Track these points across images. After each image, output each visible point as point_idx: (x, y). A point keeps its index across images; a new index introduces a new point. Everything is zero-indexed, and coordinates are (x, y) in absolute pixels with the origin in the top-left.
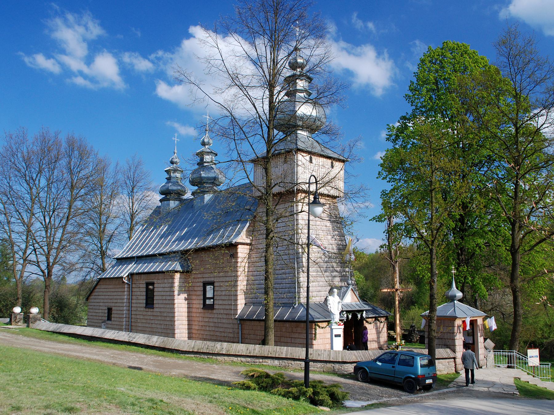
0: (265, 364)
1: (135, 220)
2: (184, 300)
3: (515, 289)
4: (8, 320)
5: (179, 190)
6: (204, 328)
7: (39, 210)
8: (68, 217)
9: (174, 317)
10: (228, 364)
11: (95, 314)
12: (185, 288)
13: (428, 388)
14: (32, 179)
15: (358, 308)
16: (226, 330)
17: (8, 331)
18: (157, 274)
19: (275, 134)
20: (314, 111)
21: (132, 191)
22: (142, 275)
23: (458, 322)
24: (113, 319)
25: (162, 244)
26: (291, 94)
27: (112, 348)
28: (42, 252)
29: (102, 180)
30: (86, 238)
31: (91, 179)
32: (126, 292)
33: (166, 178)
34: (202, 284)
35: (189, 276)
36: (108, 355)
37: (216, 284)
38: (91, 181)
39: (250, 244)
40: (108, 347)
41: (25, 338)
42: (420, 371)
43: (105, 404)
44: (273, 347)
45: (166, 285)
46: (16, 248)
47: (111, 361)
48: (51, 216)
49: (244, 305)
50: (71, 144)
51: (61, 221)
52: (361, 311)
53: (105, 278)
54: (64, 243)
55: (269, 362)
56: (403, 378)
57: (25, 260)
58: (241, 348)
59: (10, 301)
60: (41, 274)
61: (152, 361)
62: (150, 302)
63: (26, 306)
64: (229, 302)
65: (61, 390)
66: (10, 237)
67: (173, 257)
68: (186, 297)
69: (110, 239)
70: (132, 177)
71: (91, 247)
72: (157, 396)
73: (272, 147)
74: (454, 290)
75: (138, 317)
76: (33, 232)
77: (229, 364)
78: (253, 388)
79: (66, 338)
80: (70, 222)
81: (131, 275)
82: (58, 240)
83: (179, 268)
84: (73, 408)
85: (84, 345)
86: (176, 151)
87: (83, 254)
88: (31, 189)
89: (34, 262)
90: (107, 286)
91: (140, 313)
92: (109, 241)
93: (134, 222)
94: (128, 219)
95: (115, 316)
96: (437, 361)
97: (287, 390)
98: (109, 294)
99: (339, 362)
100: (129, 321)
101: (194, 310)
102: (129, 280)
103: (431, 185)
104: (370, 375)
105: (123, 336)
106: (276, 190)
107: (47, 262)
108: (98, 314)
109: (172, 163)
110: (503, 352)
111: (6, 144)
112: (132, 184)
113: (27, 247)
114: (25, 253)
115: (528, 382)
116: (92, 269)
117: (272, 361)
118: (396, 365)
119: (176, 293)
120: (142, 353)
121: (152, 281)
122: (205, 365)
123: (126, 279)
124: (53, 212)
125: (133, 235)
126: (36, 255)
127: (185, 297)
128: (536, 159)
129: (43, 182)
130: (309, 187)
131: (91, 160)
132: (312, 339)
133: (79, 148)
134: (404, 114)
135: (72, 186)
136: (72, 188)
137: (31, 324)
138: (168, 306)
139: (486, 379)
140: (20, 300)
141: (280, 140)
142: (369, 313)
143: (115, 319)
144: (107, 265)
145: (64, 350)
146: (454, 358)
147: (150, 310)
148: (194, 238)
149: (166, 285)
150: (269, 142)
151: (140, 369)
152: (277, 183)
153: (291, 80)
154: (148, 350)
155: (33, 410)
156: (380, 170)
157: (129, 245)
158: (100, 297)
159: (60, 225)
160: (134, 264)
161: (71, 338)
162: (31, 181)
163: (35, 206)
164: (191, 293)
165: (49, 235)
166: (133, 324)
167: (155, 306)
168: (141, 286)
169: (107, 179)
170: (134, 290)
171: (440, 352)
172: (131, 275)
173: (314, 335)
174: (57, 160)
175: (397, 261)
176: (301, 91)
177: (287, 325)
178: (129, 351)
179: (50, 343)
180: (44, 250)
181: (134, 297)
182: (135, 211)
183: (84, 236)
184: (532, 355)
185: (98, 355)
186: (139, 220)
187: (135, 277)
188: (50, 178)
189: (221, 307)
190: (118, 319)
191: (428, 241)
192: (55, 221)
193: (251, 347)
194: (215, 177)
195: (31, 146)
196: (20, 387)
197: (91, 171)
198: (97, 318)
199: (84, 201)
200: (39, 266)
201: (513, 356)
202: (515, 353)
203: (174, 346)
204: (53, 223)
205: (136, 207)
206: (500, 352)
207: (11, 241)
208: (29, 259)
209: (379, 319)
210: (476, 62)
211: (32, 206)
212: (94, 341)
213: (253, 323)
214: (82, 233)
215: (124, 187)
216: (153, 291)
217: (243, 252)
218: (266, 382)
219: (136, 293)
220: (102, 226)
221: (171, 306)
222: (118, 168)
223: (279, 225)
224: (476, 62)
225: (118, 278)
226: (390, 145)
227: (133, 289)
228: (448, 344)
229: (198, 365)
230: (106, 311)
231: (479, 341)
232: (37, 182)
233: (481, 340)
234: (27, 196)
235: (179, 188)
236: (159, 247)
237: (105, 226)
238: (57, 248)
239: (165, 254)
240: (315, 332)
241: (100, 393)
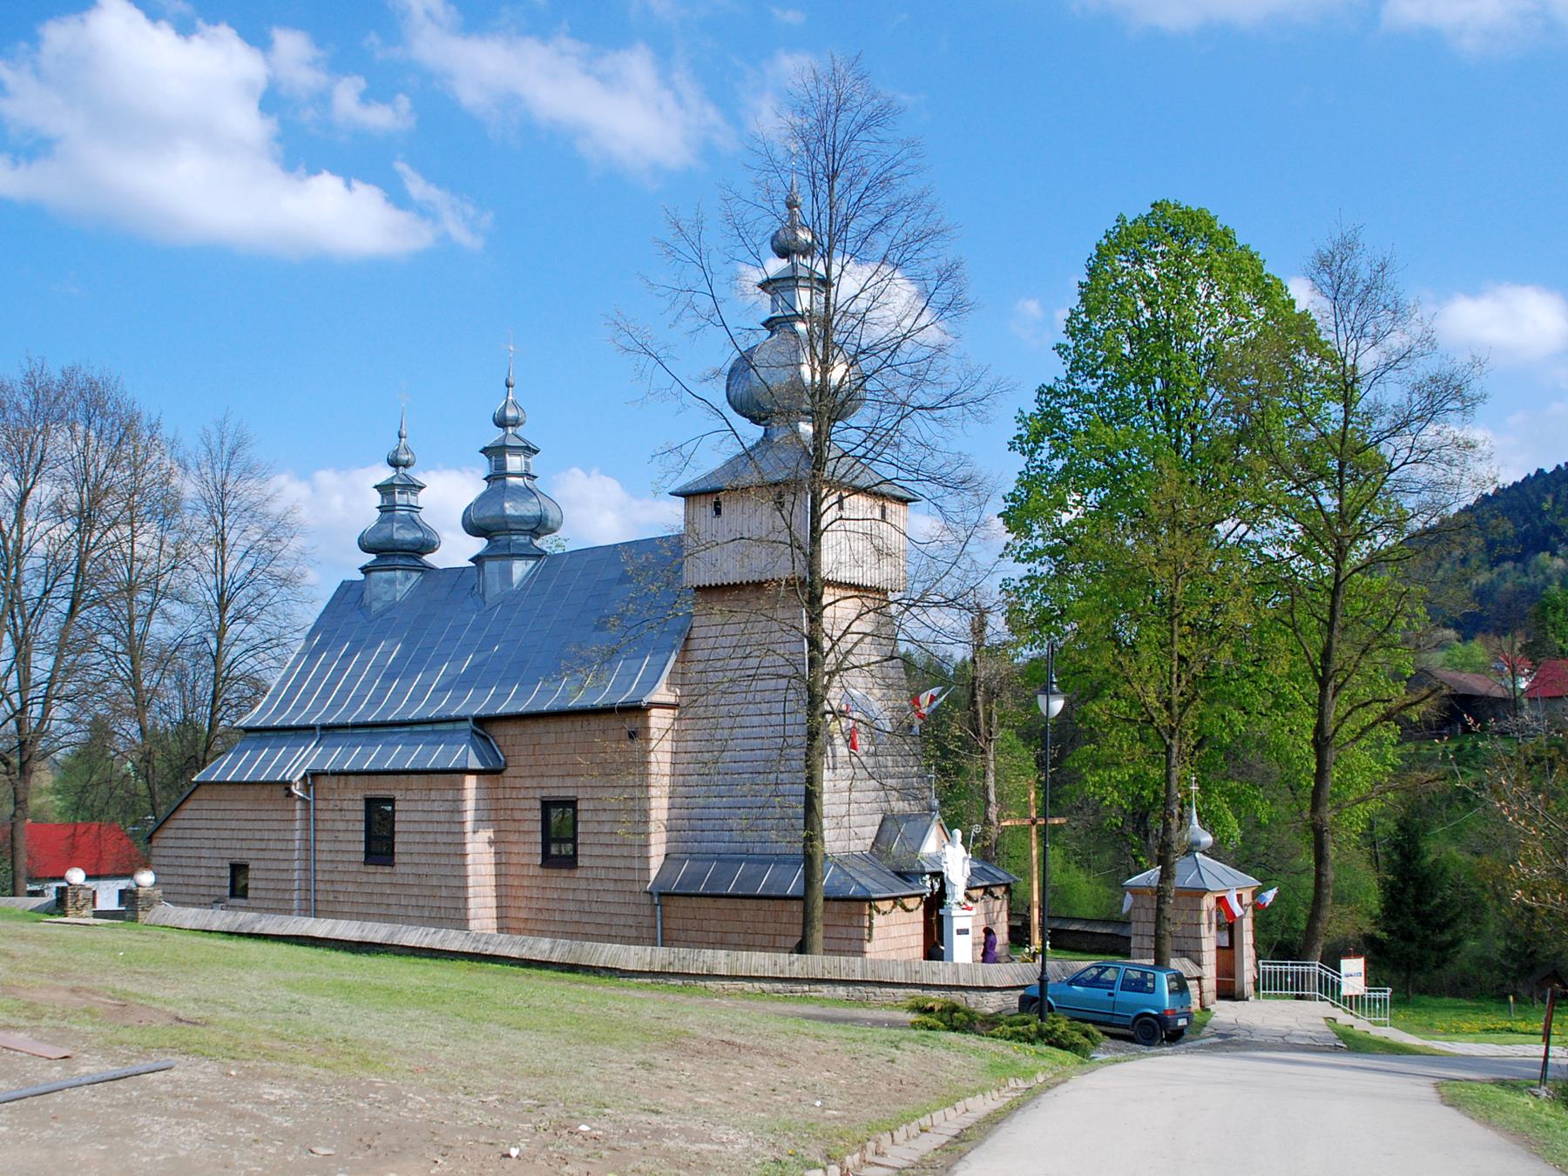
2: (487, 845)
6: (545, 915)
9: (466, 887)
12: (492, 814)
16: (615, 920)
18: (404, 777)
22: (352, 778)
23: (1209, 902)
34: (538, 805)
45: (436, 806)
49: (663, 857)
55: (825, 990)
56: (1133, 1016)
62: (379, 848)
68: (493, 837)
98: (234, 825)
102: (306, 788)
110: (1292, 965)
115: (1352, 1026)
117: (831, 988)
118: (1117, 991)
119: (469, 827)
121: (387, 793)
127: (489, 838)
132: (862, 940)
134: (1050, 383)
146: (1199, 979)
147: (380, 869)
156: (1010, 540)
158: (197, 834)
164: (503, 826)
167: (397, 859)
170: (320, 815)
173: (866, 931)
184: (1348, 972)
198: (191, 890)
202: (1317, 968)
203: (603, 958)
206: (1286, 964)
213: (694, 902)
217: (659, 720)
228: (1186, 947)
230: (227, 873)
231: (1245, 942)
235: (420, 535)
240: (871, 923)
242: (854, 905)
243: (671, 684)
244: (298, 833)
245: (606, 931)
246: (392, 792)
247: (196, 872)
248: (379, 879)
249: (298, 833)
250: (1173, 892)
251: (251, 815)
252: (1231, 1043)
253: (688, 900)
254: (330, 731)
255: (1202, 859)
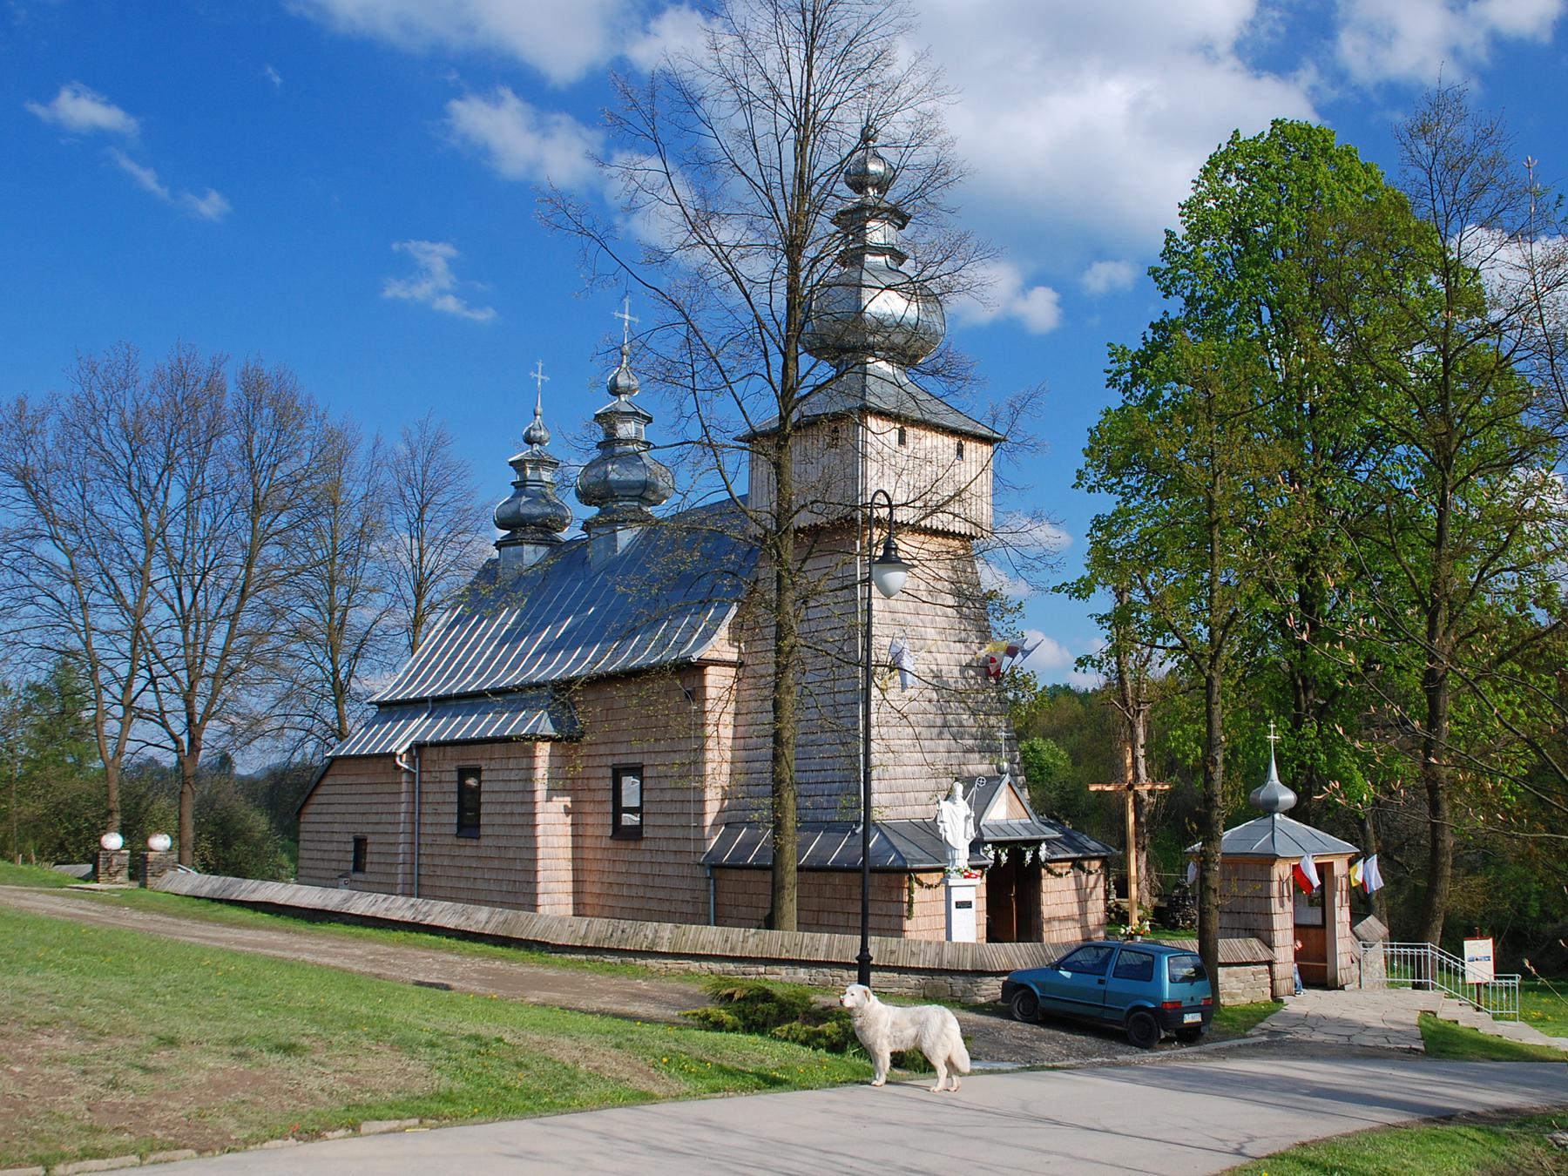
0: (774, 977)
1: (428, 597)
3: (1435, 783)
4: (88, 868)
5: (546, 515)
6: (615, 890)
7: (164, 572)
8: (243, 591)
9: (535, 860)
10: (674, 979)
11: (319, 855)
13: (1190, 1036)
14: (147, 486)
15: (1026, 836)
16: (676, 895)
17: (93, 896)
18: (488, 746)
19: (801, 374)
20: (914, 306)
21: (420, 518)
22: (449, 749)
23: (1282, 870)
24: (368, 868)
25: (502, 663)
26: (853, 257)
27: (368, 939)
28: (174, 685)
29: (337, 485)
30: (294, 647)
31: (306, 484)
32: (403, 796)
33: (513, 484)
34: (609, 773)
35: (576, 749)
36: (360, 957)
37: (647, 772)
38: (305, 490)
39: (739, 665)
40: (359, 936)
41: (138, 915)
42: (1168, 991)
43: (365, 1043)
44: (794, 933)
45: (513, 775)
46: (103, 676)
47: (368, 970)
48: (198, 588)
50: (253, 389)
51: (224, 600)
52: (1035, 844)
53: (347, 758)
54: (234, 661)
56: (1126, 1009)
57: (128, 707)
58: (710, 937)
59: (87, 820)
60: (173, 746)
61: (475, 971)
62: (469, 824)
63: (135, 832)
64: (683, 820)
65: (260, 1012)
66: (87, 644)
67: (532, 698)
68: (569, 805)
69: (358, 650)
70: (420, 478)
71: (306, 672)
72: (488, 1030)
73: (793, 408)
74: (1273, 786)
75: (437, 861)
76: (150, 630)
77: (679, 979)
78: (729, 1026)
79: (248, 915)
80: (249, 604)
81: (418, 748)
82: (217, 653)
83: (547, 728)
84: (295, 1045)
85: (295, 932)
86: (539, 410)
87: (284, 691)
88: (144, 513)
89: (150, 712)
90: (351, 778)
91: (445, 851)
92: (356, 656)
93: (424, 604)
94: (410, 595)
95: (375, 858)
96: (1221, 971)
97: (811, 1028)
98: (357, 799)
99: (964, 973)
100: (412, 874)
101: (588, 842)
102: (411, 761)
103: (1210, 509)
104: (1042, 1003)
105: (399, 908)
106: (803, 520)
107: (188, 714)
108: (326, 856)
109: (529, 441)
110: (1398, 947)
111: (78, 389)
112: (418, 498)
113: (132, 673)
114: (127, 688)
115: (1457, 1022)
116: (309, 731)
117: (791, 971)
119: (541, 795)
120: (450, 950)
121: (475, 763)
122: (614, 981)
123: (404, 759)
124: (203, 578)
125: (421, 638)
126: (157, 693)
128: (1493, 441)
129: (176, 495)
130: (891, 513)
131: (307, 432)
133: (275, 399)
135: (255, 502)
136: (257, 507)
137: (150, 880)
138: (519, 832)
139: (1346, 1015)
140: (117, 817)
141: (819, 387)
142: (1055, 849)
143: (376, 868)
144: (349, 723)
145: (244, 944)
146: (1270, 963)
147: (468, 842)
148: (591, 644)
149: (513, 775)
150: (786, 396)
151: (447, 988)
152: (806, 505)
153: (851, 222)
154: (466, 944)
155: (205, 1045)
157: (412, 667)
158: (332, 809)
159: (223, 612)
160: (427, 718)
161: (259, 914)
162: (143, 491)
163: (155, 562)
164: (581, 795)
165: (191, 639)
166: (424, 881)
167: (483, 831)
168: (446, 777)
169: (349, 485)
170: (425, 788)
171: (1228, 948)
172: (418, 749)
174: (214, 433)
175: (1139, 711)
176: (879, 250)
177: (837, 879)
178: (416, 946)
179: (204, 926)
180: (178, 681)
181: (426, 809)
182: (428, 572)
183: (288, 642)
185: (335, 956)
186: (437, 597)
187: (429, 754)
188: (193, 482)
189: (660, 833)
190: (383, 868)
191: (1202, 656)
192: (207, 603)
193: (737, 933)
194: (646, 481)
195: (146, 397)
196: (165, 1003)
197: (308, 465)
198: (326, 865)
199: (286, 546)
200: (164, 725)
201: (1426, 957)
203: (535, 931)
204: (201, 605)
205: (430, 559)
207: (91, 654)
208: (139, 706)
209: (1086, 864)
210: (1348, 178)
211: (147, 562)
212: (321, 921)
213: (745, 875)
214: (281, 633)
215: (398, 507)
216: (477, 791)
217: (717, 681)
218: (763, 1013)
219: (431, 798)
220: (337, 615)
221: (527, 831)
222: (380, 455)
223: (812, 614)
224: (1348, 178)
225: (380, 756)
226: (1115, 399)
227: (424, 786)
229: (597, 981)
230: (351, 847)
231: (1337, 919)
232: (160, 495)
233: (1342, 915)
234: (132, 532)
236: (496, 671)
237: (344, 614)
238: (214, 677)
239: (511, 691)
240: (911, 898)
241: (351, 1022)
242: (893, 876)
243: (734, 639)
244: (403, 806)
245: (666, 907)
246: (480, 762)
247: (329, 847)
248: (468, 852)
249: (403, 806)
250: (1219, 858)
251: (369, 789)
252: (1282, 1044)
253: (739, 872)
254: (440, 704)
255: (1284, 821)
